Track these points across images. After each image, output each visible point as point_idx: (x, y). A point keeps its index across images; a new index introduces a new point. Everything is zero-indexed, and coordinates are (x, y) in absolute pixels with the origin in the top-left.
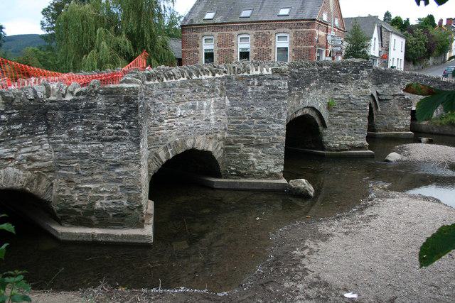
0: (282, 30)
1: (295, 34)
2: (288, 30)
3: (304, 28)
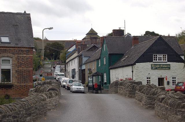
0: (6, 55)
1: (18, 58)
2: (11, 55)
3: (25, 54)
